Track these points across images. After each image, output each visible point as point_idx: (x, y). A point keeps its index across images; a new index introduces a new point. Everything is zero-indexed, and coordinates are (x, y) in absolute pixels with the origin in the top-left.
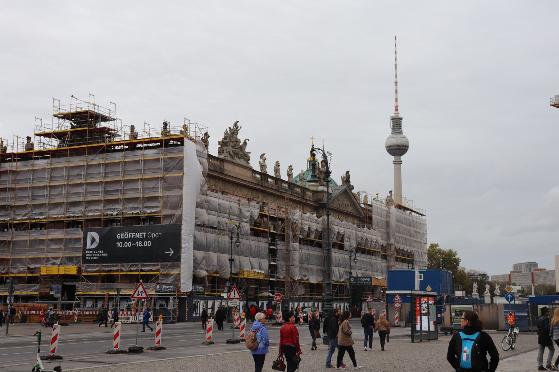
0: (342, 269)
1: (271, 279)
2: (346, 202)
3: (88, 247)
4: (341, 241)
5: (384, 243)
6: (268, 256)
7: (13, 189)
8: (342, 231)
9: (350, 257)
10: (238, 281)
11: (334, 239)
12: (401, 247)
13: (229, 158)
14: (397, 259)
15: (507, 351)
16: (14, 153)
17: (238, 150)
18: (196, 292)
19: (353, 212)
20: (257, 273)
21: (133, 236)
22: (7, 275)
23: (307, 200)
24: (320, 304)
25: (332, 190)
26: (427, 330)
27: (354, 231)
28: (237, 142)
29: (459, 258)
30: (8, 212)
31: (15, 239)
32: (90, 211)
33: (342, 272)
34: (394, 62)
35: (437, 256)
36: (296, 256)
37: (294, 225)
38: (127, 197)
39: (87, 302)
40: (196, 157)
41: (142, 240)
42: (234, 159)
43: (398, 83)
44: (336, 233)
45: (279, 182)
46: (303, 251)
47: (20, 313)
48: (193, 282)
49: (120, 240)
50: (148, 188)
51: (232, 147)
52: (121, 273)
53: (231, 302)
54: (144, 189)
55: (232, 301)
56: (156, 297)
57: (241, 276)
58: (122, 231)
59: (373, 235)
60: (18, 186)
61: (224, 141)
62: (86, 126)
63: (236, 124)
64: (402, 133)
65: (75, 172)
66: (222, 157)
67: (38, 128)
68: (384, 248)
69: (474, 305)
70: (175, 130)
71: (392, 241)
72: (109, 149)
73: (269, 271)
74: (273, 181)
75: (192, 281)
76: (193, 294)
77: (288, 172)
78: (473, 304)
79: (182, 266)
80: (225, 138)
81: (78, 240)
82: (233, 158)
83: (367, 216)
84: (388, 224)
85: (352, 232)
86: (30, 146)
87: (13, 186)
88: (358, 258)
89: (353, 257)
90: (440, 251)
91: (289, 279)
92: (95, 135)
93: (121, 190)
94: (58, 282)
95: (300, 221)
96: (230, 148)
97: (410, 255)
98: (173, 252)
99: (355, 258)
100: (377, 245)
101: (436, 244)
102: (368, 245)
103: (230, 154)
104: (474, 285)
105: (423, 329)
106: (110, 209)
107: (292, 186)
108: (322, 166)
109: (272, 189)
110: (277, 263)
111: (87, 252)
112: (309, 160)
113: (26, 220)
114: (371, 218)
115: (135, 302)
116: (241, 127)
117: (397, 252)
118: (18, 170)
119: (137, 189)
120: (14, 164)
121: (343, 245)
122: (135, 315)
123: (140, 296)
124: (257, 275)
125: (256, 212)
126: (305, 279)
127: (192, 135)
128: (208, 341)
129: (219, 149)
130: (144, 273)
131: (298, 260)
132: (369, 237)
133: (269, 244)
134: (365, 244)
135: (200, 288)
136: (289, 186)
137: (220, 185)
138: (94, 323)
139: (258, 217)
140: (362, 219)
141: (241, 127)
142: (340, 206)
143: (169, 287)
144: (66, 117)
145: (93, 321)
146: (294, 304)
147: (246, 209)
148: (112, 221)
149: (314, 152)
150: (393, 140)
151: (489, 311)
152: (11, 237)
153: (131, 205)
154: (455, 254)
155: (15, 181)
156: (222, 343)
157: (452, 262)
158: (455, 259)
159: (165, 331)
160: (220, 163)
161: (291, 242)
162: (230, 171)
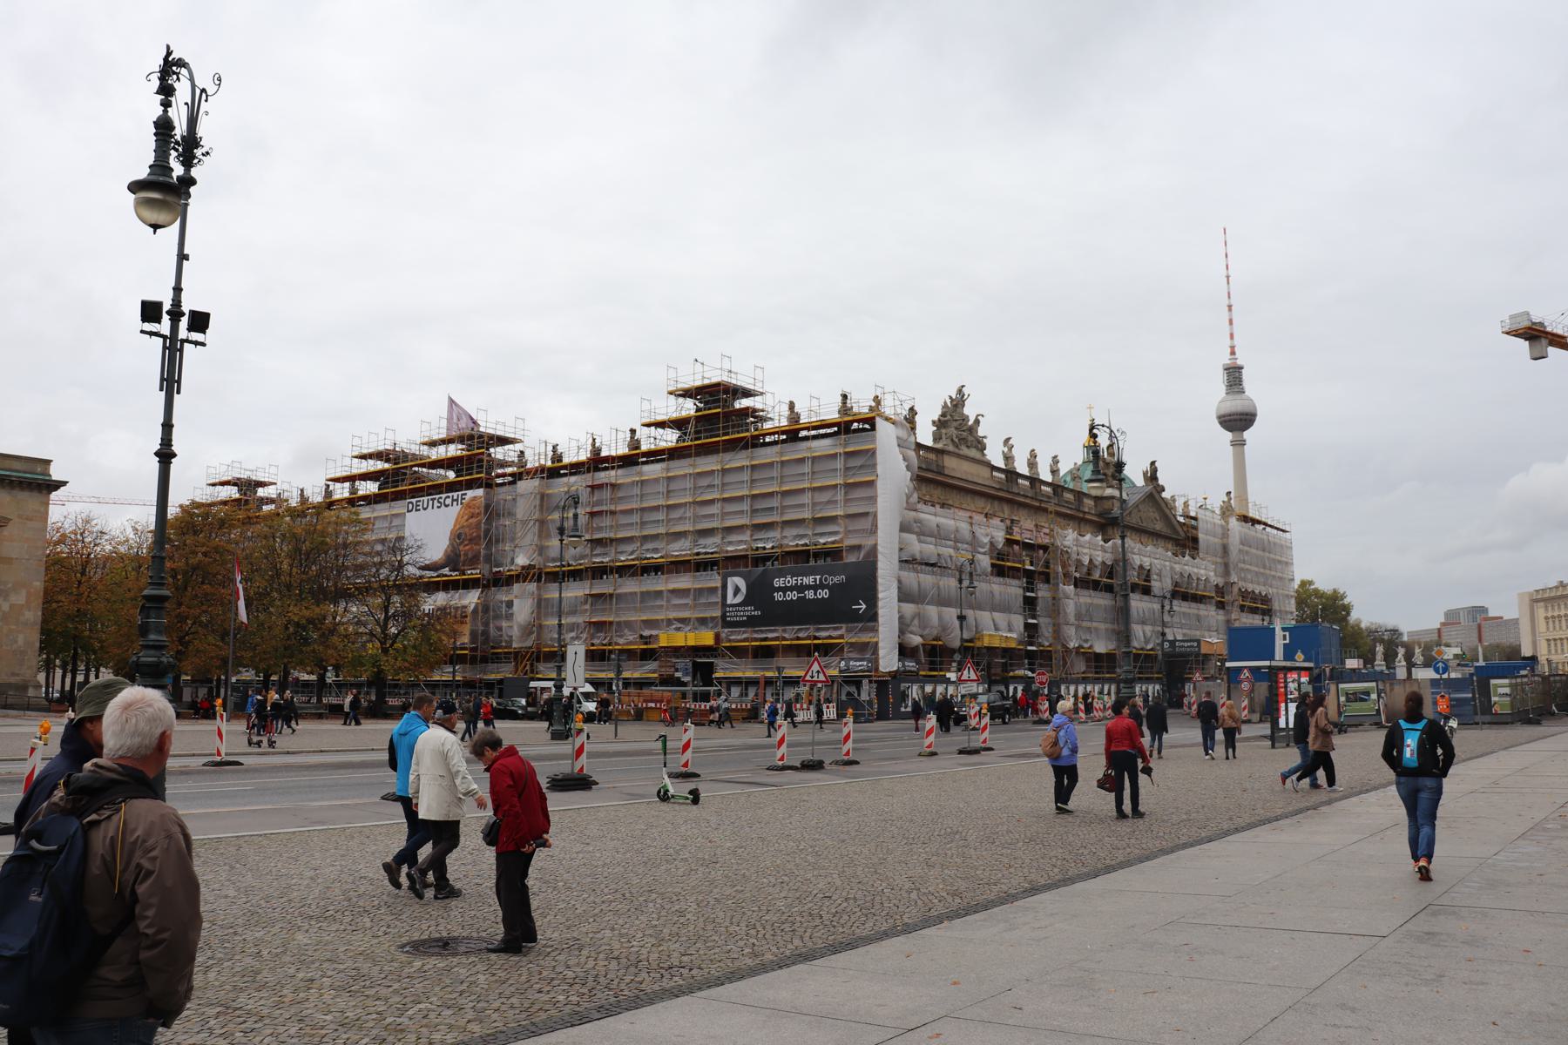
0: (1148, 629)
1: (1029, 648)
3: (729, 602)
5: (1220, 581)
6: (1022, 609)
7: (613, 513)
8: (1148, 564)
9: (1163, 607)
11: (1133, 577)
12: (1250, 587)
13: (951, 448)
18: (905, 672)
21: (799, 582)
27: (1167, 563)
28: (964, 420)
31: (619, 591)
32: (730, 543)
36: (1070, 607)
40: (897, 448)
41: (815, 588)
42: (959, 449)
43: (1245, 374)
44: (1137, 567)
45: (1037, 484)
46: (1082, 600)
49: (779, 589)
51: (956, 428)
52: (784, 643)
53: (964, 687)
54: (814, 504)
55: (965, 685)
57: (978, 644)
58: (782, 574)
60: (619, 508)
63: (960, 391)
64: (1244, 392)
65: (704, 482)
66: (939, 446)
68: (1220, 590)
71: (1234, 578)
72: (755, 443)
73: (1026, 635)
74: (1027, 483)
77: (1051, 466)
78: (1376, 681)
79: (880, 629)
80: (943, 415)
81: (713, 590)
82: (957, 447)
84: (1225, 549)
85: (1165, 566)
86: (635, 444)
87: (613, 508)
88: (1175, 608)
89: (1167, 608)
90: (1316, 591)
91: (1059, 647)
96: (952, 431)
97: (1266, 600)
98: (864, 606)
99: (1171, 608)
100: (1208, 585)
103: (952, 440)
104: (1377, 649)
106: (761, 539)
108: (1108, 454)
111: (728, 609)
113: (633, 560)
114: (1195, 540)
115: (807, 688)
117: (1243, 597)
118: (618, 482)
120: (613, 473)
121: (1150, 586)
122: (808, 709)
123: (815, 679)
125: (1000, 536)
126: (1086, 645)
128: (928, 750)
129: (934, 433)
131: (1073, 614)
133: (1024, 588)
137: (938, 493)
144: (687, 393)
146: (1068, 688)
147: (982, 531)
149: (1095, 431)
150: (1228, 404)
152: (613, 588)
154: (1343, 597)
158: (1344, 605)
160: (937, 456)
161: (1061, 585)
162: (953, 469)
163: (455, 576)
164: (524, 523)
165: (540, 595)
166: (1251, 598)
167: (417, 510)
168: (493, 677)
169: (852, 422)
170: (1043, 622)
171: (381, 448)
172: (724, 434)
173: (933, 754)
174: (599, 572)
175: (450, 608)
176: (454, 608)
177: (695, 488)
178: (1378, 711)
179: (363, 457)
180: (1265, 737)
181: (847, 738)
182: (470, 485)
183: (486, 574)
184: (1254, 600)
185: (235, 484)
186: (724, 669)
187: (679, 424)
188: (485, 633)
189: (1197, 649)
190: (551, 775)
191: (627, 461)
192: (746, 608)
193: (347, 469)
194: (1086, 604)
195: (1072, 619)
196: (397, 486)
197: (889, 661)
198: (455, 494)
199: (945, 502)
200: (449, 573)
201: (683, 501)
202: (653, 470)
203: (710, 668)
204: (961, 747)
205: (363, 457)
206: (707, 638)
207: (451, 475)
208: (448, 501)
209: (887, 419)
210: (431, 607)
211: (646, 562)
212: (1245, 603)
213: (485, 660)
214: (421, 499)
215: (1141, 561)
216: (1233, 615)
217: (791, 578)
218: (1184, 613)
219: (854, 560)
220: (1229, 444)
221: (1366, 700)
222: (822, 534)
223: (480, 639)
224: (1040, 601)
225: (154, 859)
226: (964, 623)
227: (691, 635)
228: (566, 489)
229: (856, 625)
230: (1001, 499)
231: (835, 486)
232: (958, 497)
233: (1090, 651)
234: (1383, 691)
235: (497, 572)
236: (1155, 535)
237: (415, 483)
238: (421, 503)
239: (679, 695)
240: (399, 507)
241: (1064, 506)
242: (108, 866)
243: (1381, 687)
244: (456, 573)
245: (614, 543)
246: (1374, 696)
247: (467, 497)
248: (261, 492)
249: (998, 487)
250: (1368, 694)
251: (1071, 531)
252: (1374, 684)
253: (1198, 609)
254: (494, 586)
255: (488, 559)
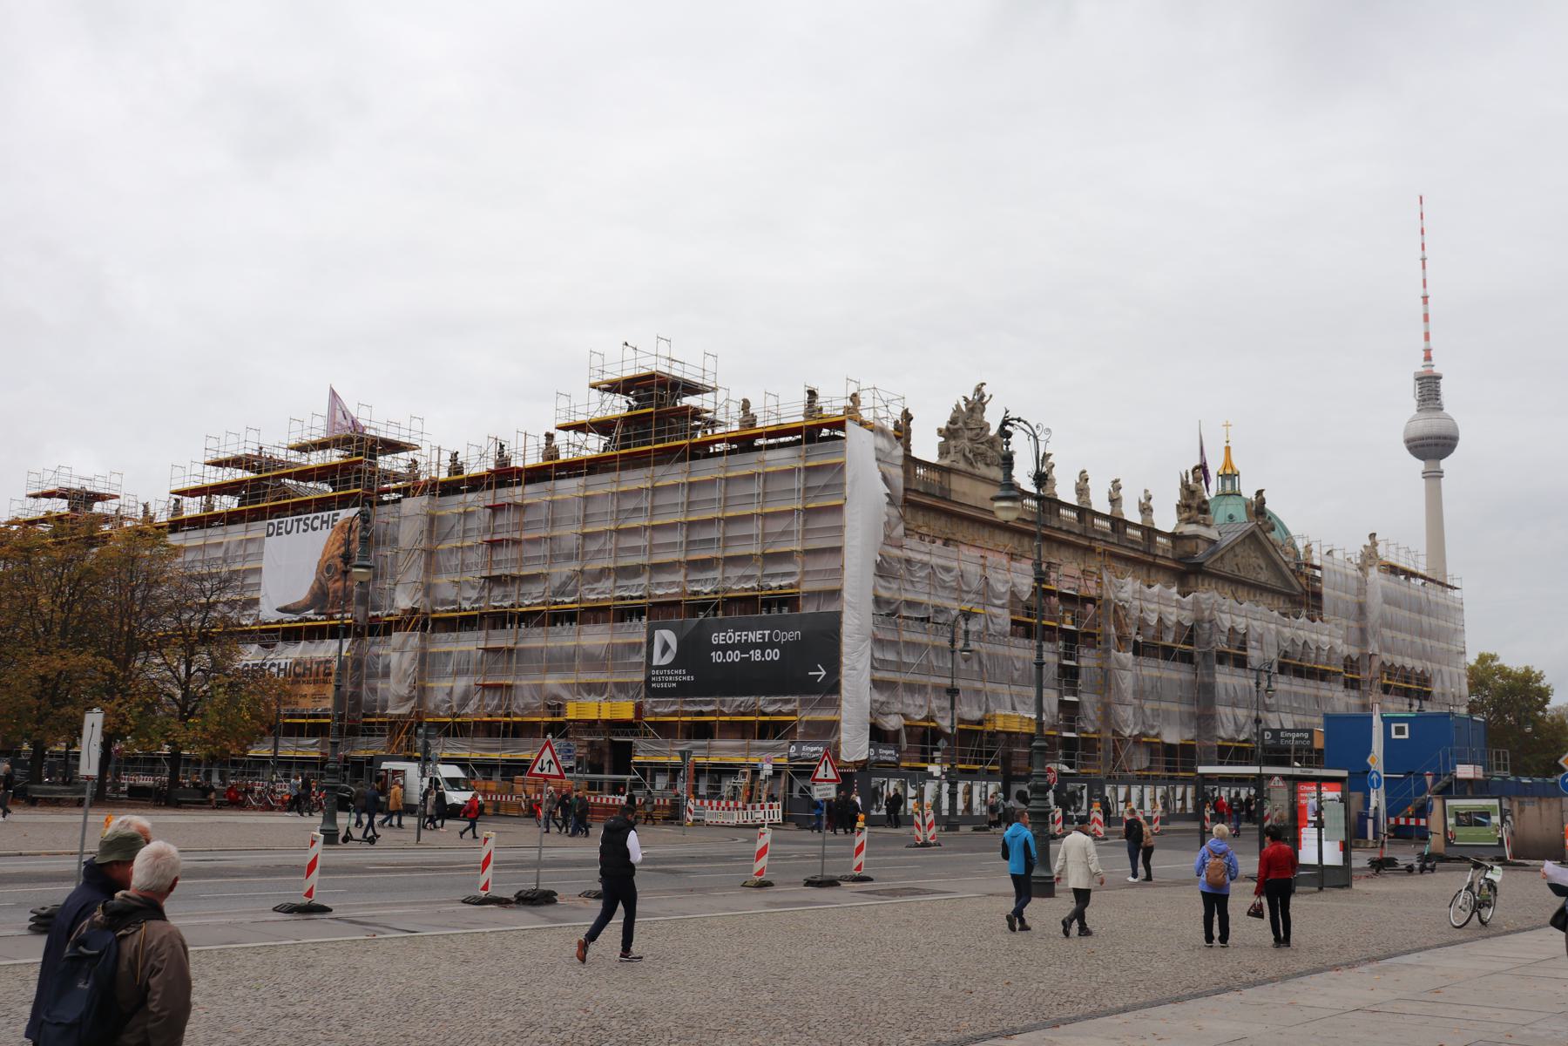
0: (1241, 713)
1: (1066, 734)
2: (1256, 560)
3: (655, 663)
4: (1239, 648)
5: (1354, 652)
6: (1056, 683)
7: (517, 542)
8: (1243, 626)
9: (1258, 684)
10: (981, 736)
11: (1221, 643)
12: (1399, 661)
13: (962, 465)
14: (1386, 689)
15: (1458, 930)
16: (518, 468)
17: (983, 447)
18: (878, 762)
19: (1274, 582)
20: (1027, 721)
21: (744, 638)
22: (508, 719)
23: (1156, 555)
24: (1190, 791)
25: (1220, 534)
26: (1316, 862)
27: (1272, 626)
28: (982, 429)
29: (1548, 686)
30: (509, 589)
31: (520, 645)
32: (659, 585)
33: (1242, 720)
34: (1419, 254)
35: (1495, 682)
36: (1127, 681)
37: (1120, 613)
38: (732, 554)
39: (657, 777)
40: (875, 464)
41: (762, 646)
42: (973, 467)
43: (1429, 299)
44: (1226, 630)
45: (1088, 518)
46: (1145, 672)
47: (524, 797)
48: (871, 739)
49: (718, 647)
50: (772, 534)
51: (971, 440)
52: (721, 718)
53: (818, 790)
54: (765, 535)
55: (819, 787)
56: (788, 771)
57: (989, 727)
58: (722, 627)
59: (1322, 634)
60: (527, 535)
61: (951, 426)
62: (651, 406)
63: (978, 390)
64: (1442, 409)
65: (629, 504)
66: (946, 462)
67: (563, 414)
68: (1350, 664)
69: (1504, 801)
70: (834, 404)
71: (1373, 648)
72: (700, 452)
73: (1061, 716)
74: (1073, 515)
75: (868, 737)
76: (871, 766)
77: (1110, 493)
78: (1499, 798)
79: (844, 704)
80: (953, 421)
81: (634, 648)
82: (971, 464)
83: (1307, 592)
84: (1362, 609)
85: (1269, 629)
86: (551, 452)
87: (517, 535)
88: (1274, 686)
89: (1264, 684)
90: (1501, 669)
91: (1110, 735)
92: (671, 423)
93: (719, 539)
94: (599, 735)
95: (1136, 603)
96: (965, 443)
97: (1424, 679)
98: (823, 673)
99: (1269, 686)
100: (1333, 656)
101: (1493, 653)
102: (1309, 656)
103: (964, 455)
105: (1325, 862)
106: (698, 581)
107: (1121, 525)
108: (1194, 479)
109: (1069, 532)
110: (1080, 698)
111: (653, 672)
112: (1221, 473)
113: (538, 604)
114: (1317, 596)
115: (747, 780)
116: (991, 396)
117: (1389, 674)
118: (525, 502)
119: (750, 537)
120: (518, 490)
121: (1245, 656)
122: (745, 809)
123: (546, 772)
124: (1028, 725)
125: (1026, 585)
126: (1153, 732)
127: (867, 415)
128: (758, 878)
129: (941, 445)
130: (767, 718)
131: (1130, 691)
132: (1312, 640)
133: (1059, 654)
134: (1302, 654)
135: (888, 754)
136: (1112, 525)
137: (940, 525)
138: (666, 824)
139: (1032, 594)
140: (1298, 599)
141: (991, 396)
142: (1239, 569)
143: (815, 749)
144: (614, 387)
145: (665, 819)
146: (1116, 790)
147: (1000, 577)
148: (704, 606)
149: (1008, 428)
150: (1420, 423)
151: (1541, 815)
152: (514, 641)
153: (739, 572)
154: (1539, 678)
155: (521, 526)
156: (797, 884)
157: (1532, 696)
158: (1540, 689)
159: (778, 847)
160: (941, 477)
161: (1113, 651)
162: (964, 494)
163: (321, 620)
164: (410, 552)
165: (424, 648)
166: (1400, 676)
167: (278, 534)
168: (362, 754)
169: (820, 427)
170: (1089, 702)
171: (241, 453)
172: (657, 442)
173: (768, 884)
174: (499, 620)
175: (312, 663)
176: (316, 663)
177: (619, 511)
178: (1501, 840)
179: (218, 464)
180: (1252, 878)
181: (860, 849)
182: (344, 502)
183: (360, 619)
184: (1407, 680)
185: (62, 496)
186: (646, 752)
187: (602, 427)
188: (356, 697)
189: (1308, 742)
190: (37, 908)
191: (535, 475)
192: (676, 672)
193: (197, 478)
194: (1151, 678)
195: (1129, 697)
196: (258, 502)
197: (855, 746)
198: (326, 514)
199: (950, 536)
200: (313, 617)
201: (602, 529)
202: (569, 488)
203: (628, 749)
204: (808, 876)
205: (218, 464)
206: (624, 709)
207: (327, 489)
208: (317, 523)
209: (862, 424)
210: (289, 661)
211: (555, 607)
212: (1390, 682)
213: (353, 731)
214: (285, 519)
215: (1233, 622)
216: (1371, 698)
217: (734, 633)
218: (1296, 694)
219: (814, 611)
220: (1420, 475)
221: (1484, 824)
222: (773, 576)
223: (348, 703)
224: (1083, 672)
225: (163, 961)
226: (956, 698)
227: (606, 706)
228: (461, 510)
229: (813, 697)
230: (1032, 535)
231: (791, 512)
232: (970, 530)
233: (1158, 740)
234: (1509, 812)
235: (373, 617)
236: (1257, 588)
237: (279, 499)
238: (283, 525)
239: (584, 785)
240: (258, 529)
241: (1126, 547)
242: (133, 964)
243: (1505, 806)
244: (322, 617)
245: (518, 582)
246: (1496, 819)
247: (340, 518)
248: (98, 507)
249: (1029, 519)
250: (1487, 815)
251: (1130, 579)
252: (1495, 802)
253: (1318, 688)
254: (371, 635)
255: (363, 599)
